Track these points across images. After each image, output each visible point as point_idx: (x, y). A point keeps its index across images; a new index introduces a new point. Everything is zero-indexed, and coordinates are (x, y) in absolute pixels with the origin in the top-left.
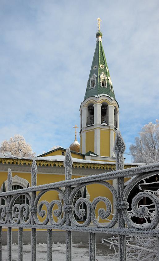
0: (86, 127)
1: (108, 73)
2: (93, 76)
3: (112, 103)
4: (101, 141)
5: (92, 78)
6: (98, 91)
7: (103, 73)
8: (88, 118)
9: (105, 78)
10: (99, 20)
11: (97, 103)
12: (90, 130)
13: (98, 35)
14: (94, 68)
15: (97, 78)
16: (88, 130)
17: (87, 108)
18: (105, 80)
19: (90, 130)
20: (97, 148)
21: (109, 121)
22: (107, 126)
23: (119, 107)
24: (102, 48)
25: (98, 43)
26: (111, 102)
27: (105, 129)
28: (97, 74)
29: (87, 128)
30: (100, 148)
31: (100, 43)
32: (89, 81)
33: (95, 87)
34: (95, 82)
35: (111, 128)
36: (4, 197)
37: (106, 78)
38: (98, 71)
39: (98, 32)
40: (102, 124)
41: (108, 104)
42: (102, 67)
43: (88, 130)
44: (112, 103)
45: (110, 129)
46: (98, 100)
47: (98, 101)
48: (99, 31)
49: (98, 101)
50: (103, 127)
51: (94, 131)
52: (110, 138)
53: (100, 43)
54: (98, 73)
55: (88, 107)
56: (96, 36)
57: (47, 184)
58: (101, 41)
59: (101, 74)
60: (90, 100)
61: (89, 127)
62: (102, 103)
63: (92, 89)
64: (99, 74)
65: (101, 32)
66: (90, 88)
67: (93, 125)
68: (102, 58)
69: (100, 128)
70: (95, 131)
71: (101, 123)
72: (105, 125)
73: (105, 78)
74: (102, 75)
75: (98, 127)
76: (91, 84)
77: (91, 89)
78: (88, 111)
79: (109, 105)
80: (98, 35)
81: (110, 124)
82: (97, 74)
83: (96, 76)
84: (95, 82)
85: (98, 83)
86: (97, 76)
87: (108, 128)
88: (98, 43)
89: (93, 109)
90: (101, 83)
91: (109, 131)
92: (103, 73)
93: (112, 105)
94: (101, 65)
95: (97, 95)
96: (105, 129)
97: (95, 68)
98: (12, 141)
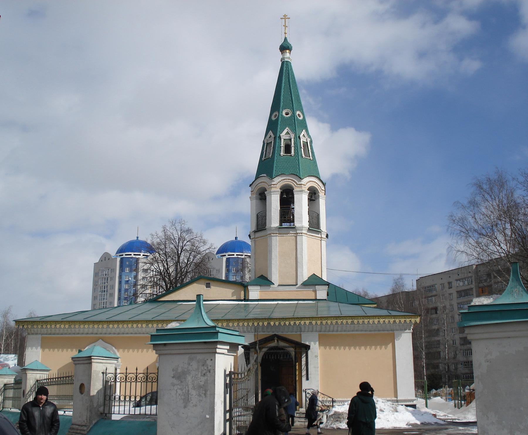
13: (285, 48)
42: (287, 114)
46: (273, 183)
53: (287, 65)
65: (291, 41)
81: (297, 224)
90: (282, 149)
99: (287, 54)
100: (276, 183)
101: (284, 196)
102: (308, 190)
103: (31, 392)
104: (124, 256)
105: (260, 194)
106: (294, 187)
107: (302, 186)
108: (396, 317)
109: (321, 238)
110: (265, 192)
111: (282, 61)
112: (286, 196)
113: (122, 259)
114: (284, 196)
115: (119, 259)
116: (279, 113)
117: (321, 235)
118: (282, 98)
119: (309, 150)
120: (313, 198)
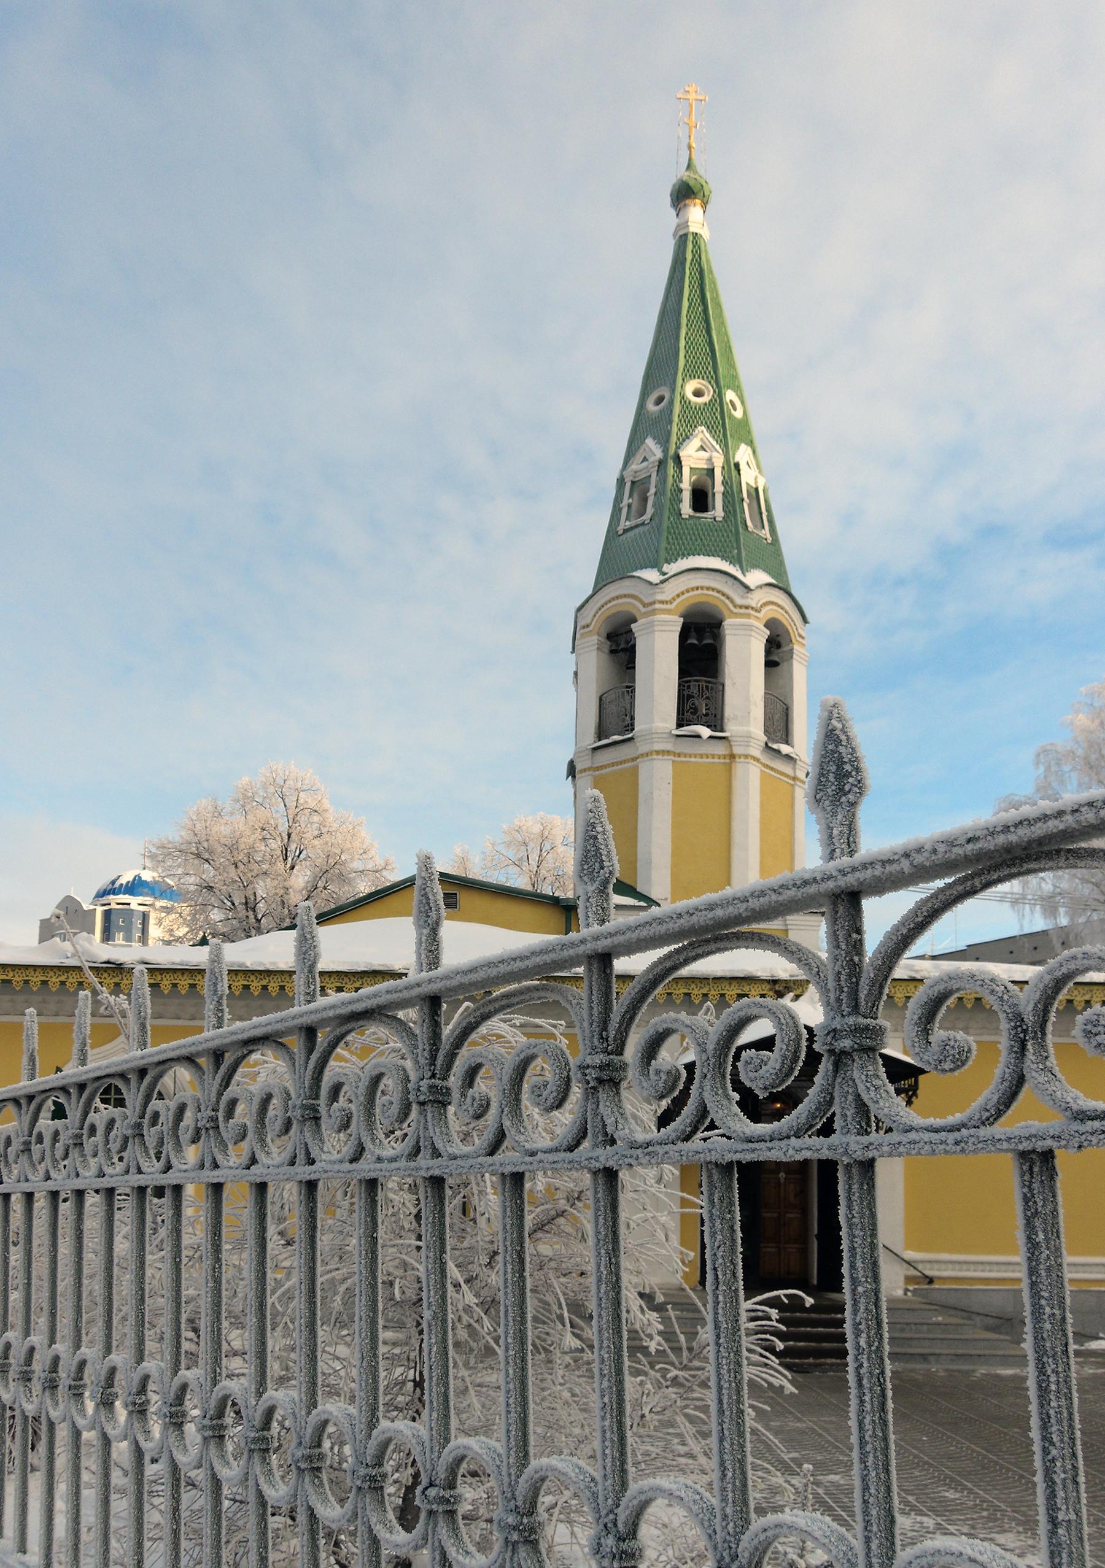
0: (595, 749)
1: (744, 423)
2: (639, 457)
3: (747, 607)
4: (676, 825)
5: (634, 467)
6: (664, 545)
7: (702, 434)
8: (612, 696)
9: (710, 460)
10: (692, 96)
11: (654, 612)
12: (613, 764)
13: (684, 194)
14: (651, 407)
15: (662, 464)
16: (605, 767)
17: (600, 644)
18: (711, 472)
19: (613, 764)
20: (649, 862)
21: (728, 711)
22: (711, 737)
23: (805, 620)
24: (701, 273)
25: (684, 240)
26: (739, 601)
27: (701, 756)
28: (664, 442)
29: (599, 752)
30: (758, 816)
31: (690, 247)
32: (621, 482)
33: (646, 517)
34: (653, 490)
35: (737, 750)
36: (64, 1089)
37: (719, 461)
38: (671, 422)
39: (682, 173)
40: (686, 730)
41: (720, 612)
42: (698, 393)
43: (605, 767)
44: (747, 607)
45: (732, 756)
46: (659, 597)
47: (662, 602)
48: (689, 167)
49: (662, 602)
50: (686, 746)
51: (636, 768)
52: (729, 803)
53: (696, 244)
54: (669, 433)
55: (609, 637)
56: (669, 199)
57: (10, 1087)
58: (705, 233)
59: (686, 438)
60: (617, 598)
61: (611, 750)
62: (682, 609)
63: (632, 528)
64: (674, 439)
65: (707, 172)
66: (624, 524)
67: (632, 739)
68: (702, 340)
69: (668, 752)
70: (644, 767)
71: (679, 725)
72: (699, 737)
73: (710, 460)
74: (694, 444)
75: (658, 747)
76: (626, 500)
77: (625, 531)
78: (605, 657)
79: (729, 624)
80: (684, 194)
81: (732, 729)
82: (664, 442)
83: (659, 454)
84: (653, 490)
85: (664, 493)
86: (665, 451)
87: (720, 749)
88: (684, 240)
89: (634, 646)
90: (687, 496)
91: (729, 769)
92: (702, 434)
93: (748, 616)
94: (691, 386)
95: (655, 565)
96: (701, 756)
97: (660, 400)
98: (246, 801)
99: (695, 214)
100: (669, 598)
101: (689, 641)
102: (767, 626)
103: (1030, 1200)
104: (114, 906)
105: (611, 636)
106: (726, 612)
107: (750, 611)
108: (1092, 987)
109: (795, 778)
110: (633, 626)
111: (681, 233)
112: (695, 642)
113: (107, 915)
114: (689, 641)
115: (100, 910)
116: (673, 391)
117: (794, 769)
118: (682, 343)
119: (761, 514)
120: (776, 658)
